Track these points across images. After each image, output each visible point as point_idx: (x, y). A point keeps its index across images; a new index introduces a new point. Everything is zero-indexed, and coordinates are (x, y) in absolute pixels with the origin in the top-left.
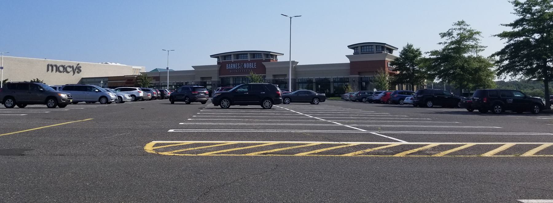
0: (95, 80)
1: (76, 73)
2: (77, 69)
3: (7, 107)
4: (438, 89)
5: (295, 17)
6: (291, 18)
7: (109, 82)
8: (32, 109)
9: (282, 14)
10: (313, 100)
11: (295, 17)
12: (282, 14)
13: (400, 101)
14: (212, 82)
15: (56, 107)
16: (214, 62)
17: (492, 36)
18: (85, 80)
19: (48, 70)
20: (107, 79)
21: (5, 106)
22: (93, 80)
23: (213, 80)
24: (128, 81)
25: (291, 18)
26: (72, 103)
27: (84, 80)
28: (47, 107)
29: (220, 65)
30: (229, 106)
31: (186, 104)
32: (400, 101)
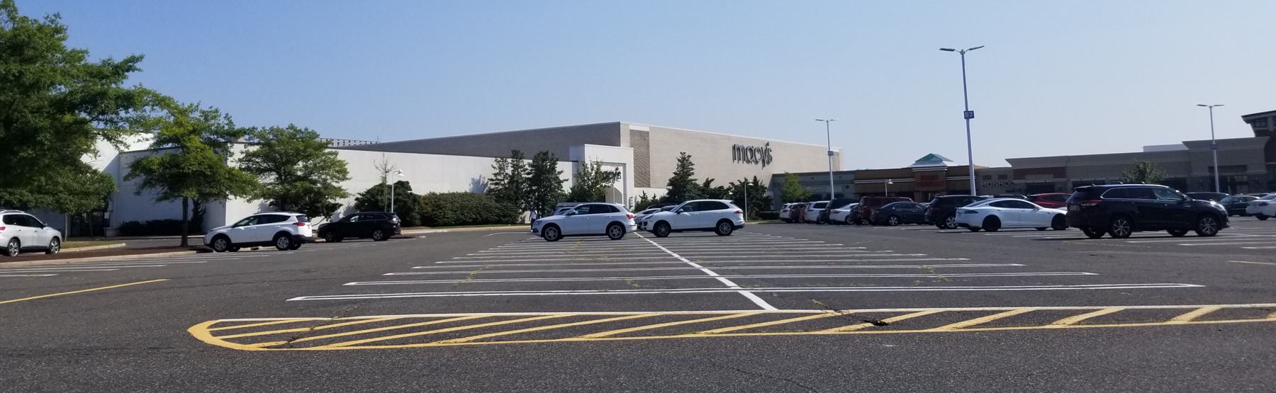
0: (813, 178)
1: (766, 164)
2: (765, 156)
3: (280, 249)
4: (1086, 187)
5: (971, 49)
6: (962, 53)
7: (856, 182)
8: (1140, 239)
9: (942, 49)
10: (889, 218)
11: (971, 49)
12: (942, 49)
13: (949, 219)
14: (1249, 176)
15: (1186, 235)
16: (1248, 132)
17: (142, 71)
18: (810, 177)
19: (734, 159)
20: (852, 177)
21: (277, 247)
22: (809, 179)
23: (1250, 172)
24: (922, 179)
25: (962, 53)
26: (983, 230)
27: (781, 180)
28: (1110, 236)
29: (1266, 138)
30: (1130, 234)
31: (327, 242)
32: (949, 219)
